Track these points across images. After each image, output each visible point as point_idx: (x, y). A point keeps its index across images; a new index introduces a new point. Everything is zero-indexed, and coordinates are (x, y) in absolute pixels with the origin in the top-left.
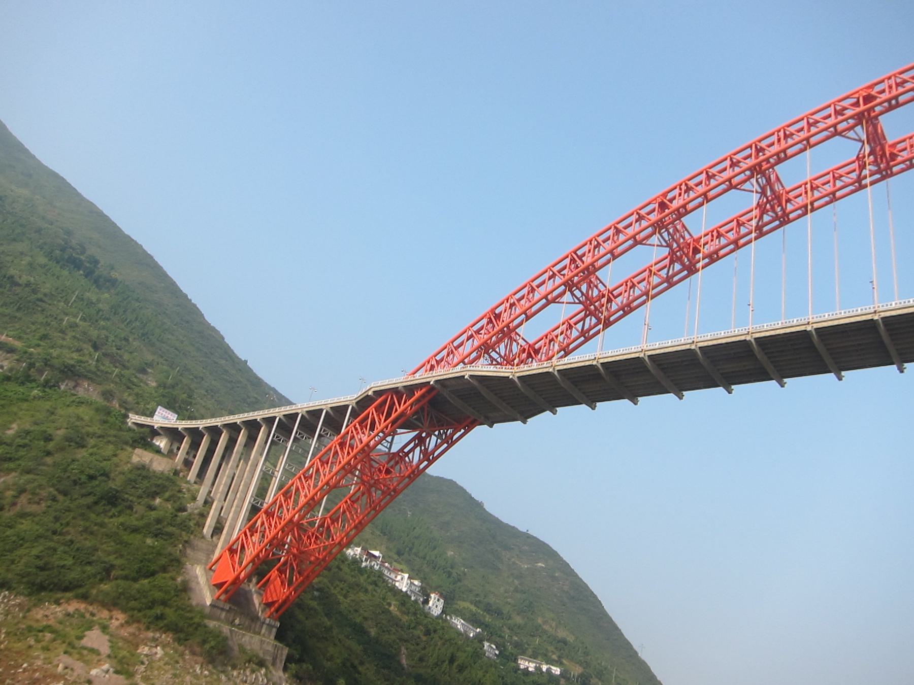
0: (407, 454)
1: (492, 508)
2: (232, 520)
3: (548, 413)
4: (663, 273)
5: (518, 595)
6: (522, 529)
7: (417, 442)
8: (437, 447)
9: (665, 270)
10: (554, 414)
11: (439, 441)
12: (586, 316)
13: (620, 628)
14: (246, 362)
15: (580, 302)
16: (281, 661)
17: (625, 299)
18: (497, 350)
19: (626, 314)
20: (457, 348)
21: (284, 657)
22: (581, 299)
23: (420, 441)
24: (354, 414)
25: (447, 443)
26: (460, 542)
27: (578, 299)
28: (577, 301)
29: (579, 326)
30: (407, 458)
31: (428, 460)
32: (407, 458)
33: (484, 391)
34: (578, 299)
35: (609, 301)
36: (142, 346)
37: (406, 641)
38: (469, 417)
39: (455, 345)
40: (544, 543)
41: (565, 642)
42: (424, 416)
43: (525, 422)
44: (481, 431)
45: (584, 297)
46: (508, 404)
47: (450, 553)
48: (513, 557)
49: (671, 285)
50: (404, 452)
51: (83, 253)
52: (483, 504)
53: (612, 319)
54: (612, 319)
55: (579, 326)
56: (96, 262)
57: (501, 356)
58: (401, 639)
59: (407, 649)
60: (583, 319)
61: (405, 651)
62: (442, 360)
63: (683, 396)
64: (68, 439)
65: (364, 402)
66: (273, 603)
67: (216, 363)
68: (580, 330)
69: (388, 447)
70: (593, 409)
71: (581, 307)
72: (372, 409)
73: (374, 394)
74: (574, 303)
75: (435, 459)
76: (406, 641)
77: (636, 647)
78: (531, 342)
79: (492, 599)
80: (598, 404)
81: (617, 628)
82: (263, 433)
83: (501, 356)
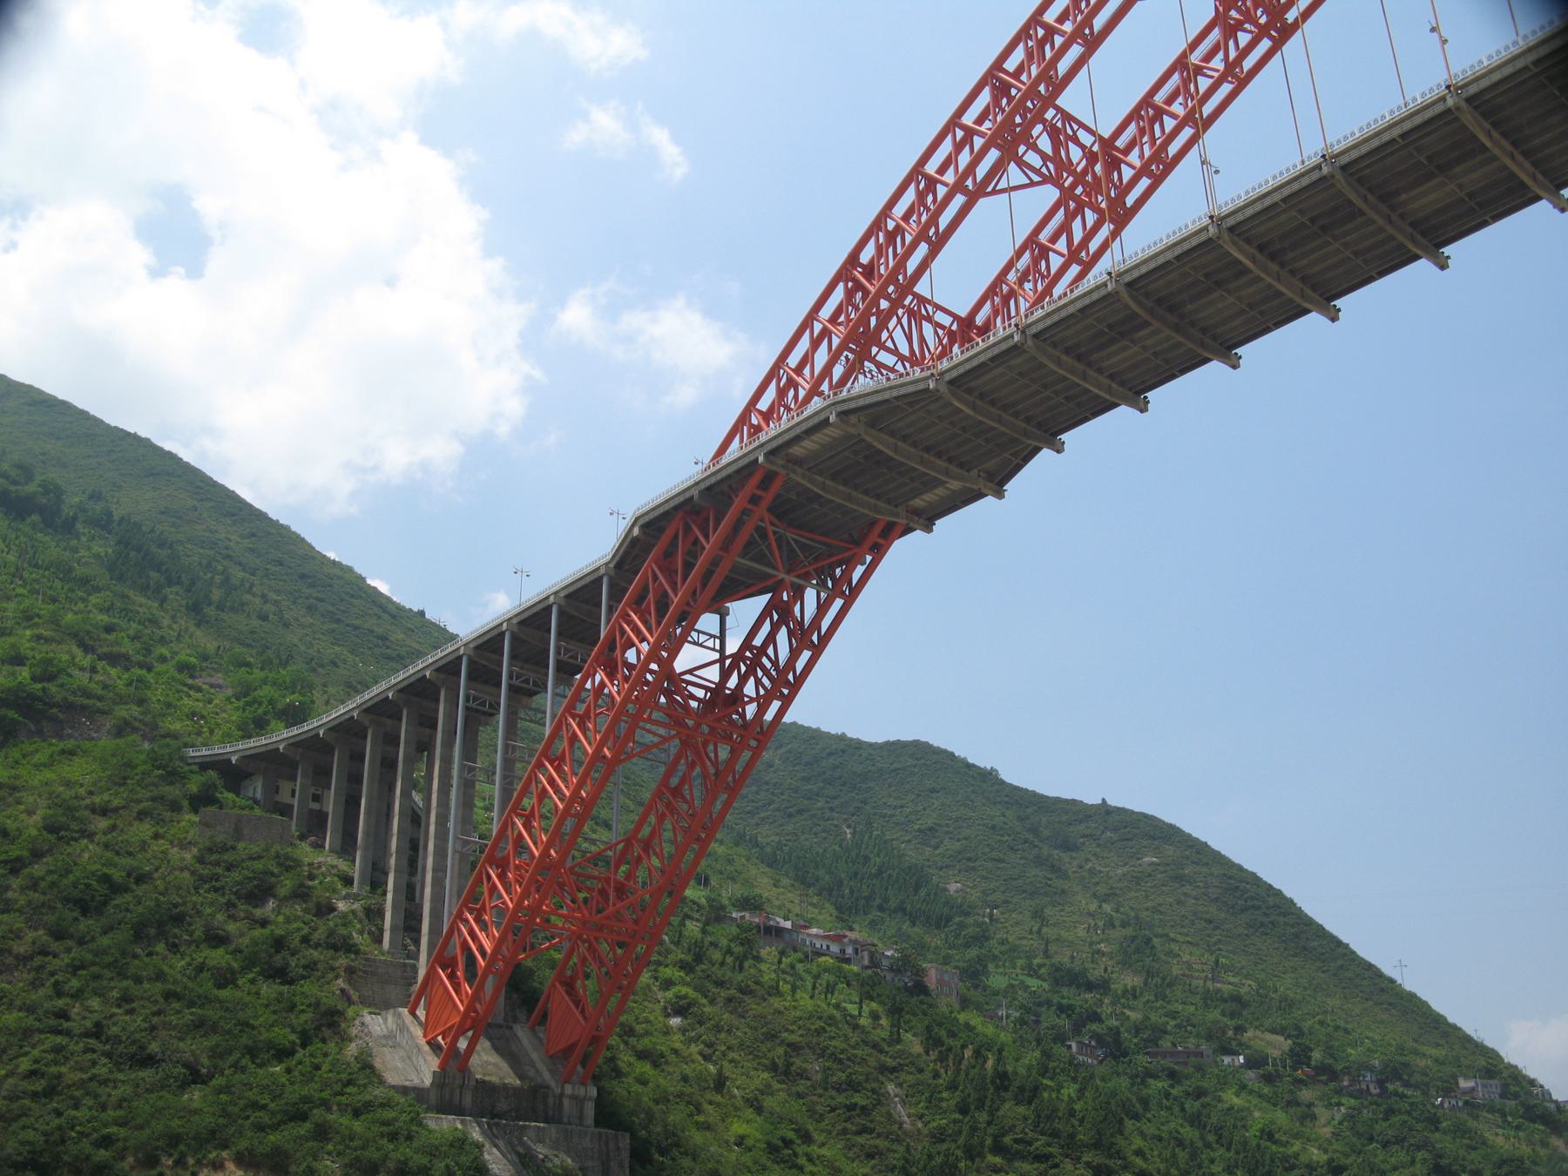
0: (762, 650)
1: (1018, 773)
2: (433, 901)
3: (1046, 454)
4: (1217, 63)
5: (1116, 934)
6: (1091, 798)
7: (776, 617)
8: (822, 608)
9: (1220, 55)
10: (1058, 452)
11: (823, 595)
12: (1070, 217)
13: (1345, 941)
14: (422, 613)
15: (1046, 180)
16: (621, 1166)
17: (1146, 148)
18: (889, 344)
19: (1147, 101)
20: (799, 370)
21: (625, 1155)
22: (1044, 170)
23: (779, 612)
24: (616, 593)
25: (842, 594)
26: (969, 859)
27: (1037, 172)
28: (1036, 178)
29: (1061, 245)
30: (765, 660)
31: (811, 646)
32: (765, 660)
33: (881, 443)
34: (1037, 172)
35: (1114, 164)
36: (192, 629)
37: (893, 1070)
38: (873, 523)
39: (793, 366)
40: (1146, 816)
41: (1237, 999)
42: (769, 547)
43: (1000, 494)
44: (907, 550)
45: (1051, 166)
46: (950, 460)
47: (953, 887)
48: (1087, 860)
49: (1242, 83)
50: (755, 647)
51: (30, 477)
52: (996, 771)
53: (1130, 201)
54: (1130, 201)
55: (1061, 245)
56: (59, 492)
57: (902, 358)
58: (883, 1069)
59: (900, 1085)
60: (1065, 228)
61: (898, 1090)
62: (771, 409)
63: (1339, 310)
64: (51, 828)
65: (631, 553)
66: (572, 1047)
67: (356, 628)
68: (1065, 251)
69: (718, 647)
70: (1143, 410)
71: (1050, 194)
72: (649, 565)
73: (645, 533)
74: (1032, 184)
75: (825, 640)
76: (893, 1070)
77: (1388, 970)
78: (963, 312)
79: (1063, 958)
80: (1151, 395)
81: (1339, 943)
82: (445, 701)
83: (902, 358)
